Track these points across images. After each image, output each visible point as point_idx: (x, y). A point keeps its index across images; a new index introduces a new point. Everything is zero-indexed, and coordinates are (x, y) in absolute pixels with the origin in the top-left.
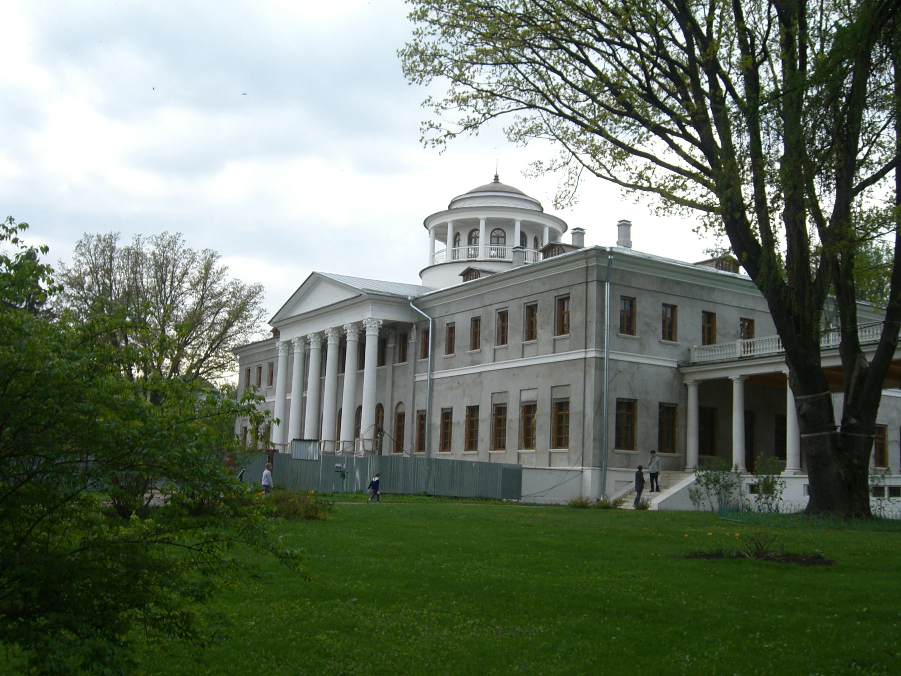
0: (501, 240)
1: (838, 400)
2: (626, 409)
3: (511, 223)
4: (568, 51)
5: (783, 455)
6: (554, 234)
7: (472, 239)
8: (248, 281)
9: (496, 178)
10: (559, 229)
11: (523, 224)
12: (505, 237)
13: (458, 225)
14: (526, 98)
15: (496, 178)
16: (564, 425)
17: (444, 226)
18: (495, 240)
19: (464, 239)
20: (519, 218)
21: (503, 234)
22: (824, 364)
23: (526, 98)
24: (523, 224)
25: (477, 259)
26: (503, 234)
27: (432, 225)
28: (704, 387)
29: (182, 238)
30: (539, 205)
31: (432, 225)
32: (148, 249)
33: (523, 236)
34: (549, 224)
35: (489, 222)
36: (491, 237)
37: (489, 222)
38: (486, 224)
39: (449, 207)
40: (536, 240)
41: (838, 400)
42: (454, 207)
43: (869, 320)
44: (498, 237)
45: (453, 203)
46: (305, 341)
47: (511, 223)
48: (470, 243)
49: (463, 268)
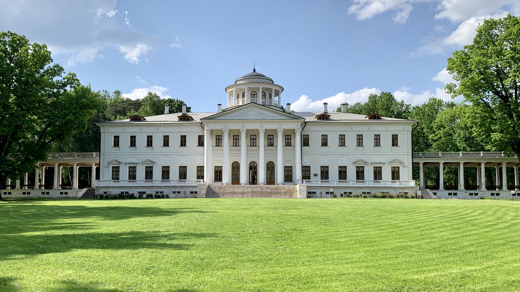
0: (255, 96)
3: (258, 89)
18: (252, 96)
19: (267, 95)
44: (254, 95)
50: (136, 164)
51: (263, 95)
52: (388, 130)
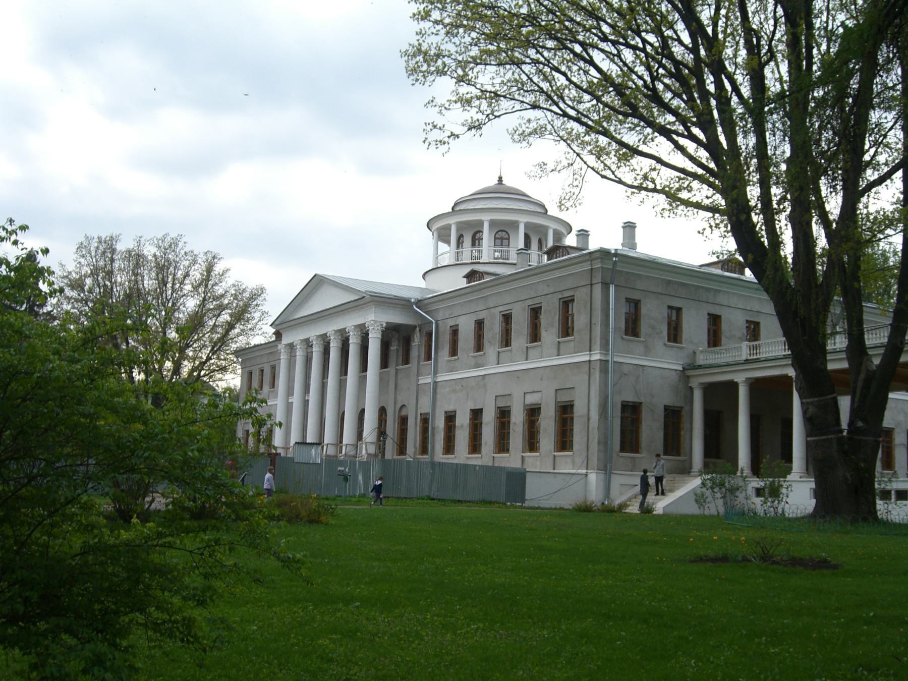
0: (505, 242)
1: (845, 403)
2: (631, 413)
3: (514, 225)
4: (572, 51)
5: (789, 458)
6: (558, 236)
7: (476, 241)
8: (250, 283)
9: (500, 179)
10: (564, 231)
11: (527, 225)
12: (509, 239)
13: (462, 226)
14: (530, 98)
15: (500, 179)
16: (568, 428)
17: (448, 228)
18: (498, 242)
19: (467, 241)
20: (523, 219)
22: (831, 366)
23: (530, 98)
24: (527, 225)
25: (481, 261)
27: (436, 226)
28: (710, 390)
29: (183, 240)
30: (543, 206)
31: (436, 226)
32: (149, 251)
33: (527, 238)
34: (553, 226)
35: (493, 223)
36: (495, 238)
37: (493, 223)
38: (490, 226)
39: (453, 208)
40: (540, 241)
41: (845, 403)
42: (458, 208)
43: (876, 322)
44: (502, 239)
45: (456, 204)
46: (308, 343)
47: (514, 225)
48: (473, 245)
49: (467, 270)
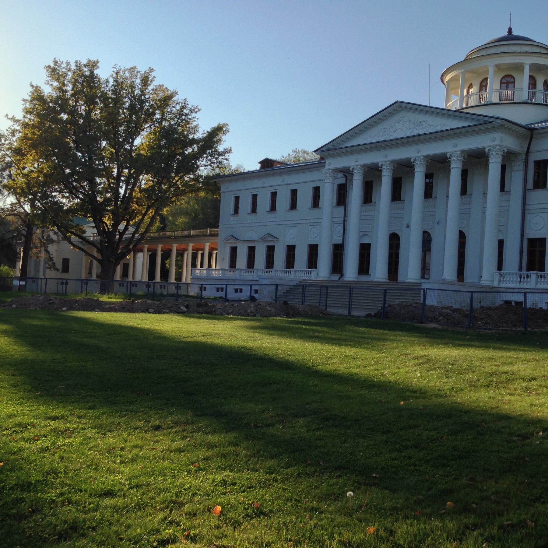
3: (519, 68)
9: (510, 30)
12: (514, 82)
15: (510, 30)
18: (504, 85)
21: (512, 80)
26: (512, 80)
29: (153, 74)
36: (501, 83)
50: (253, 241)
51: (530, 84)
52: (265, 185)
